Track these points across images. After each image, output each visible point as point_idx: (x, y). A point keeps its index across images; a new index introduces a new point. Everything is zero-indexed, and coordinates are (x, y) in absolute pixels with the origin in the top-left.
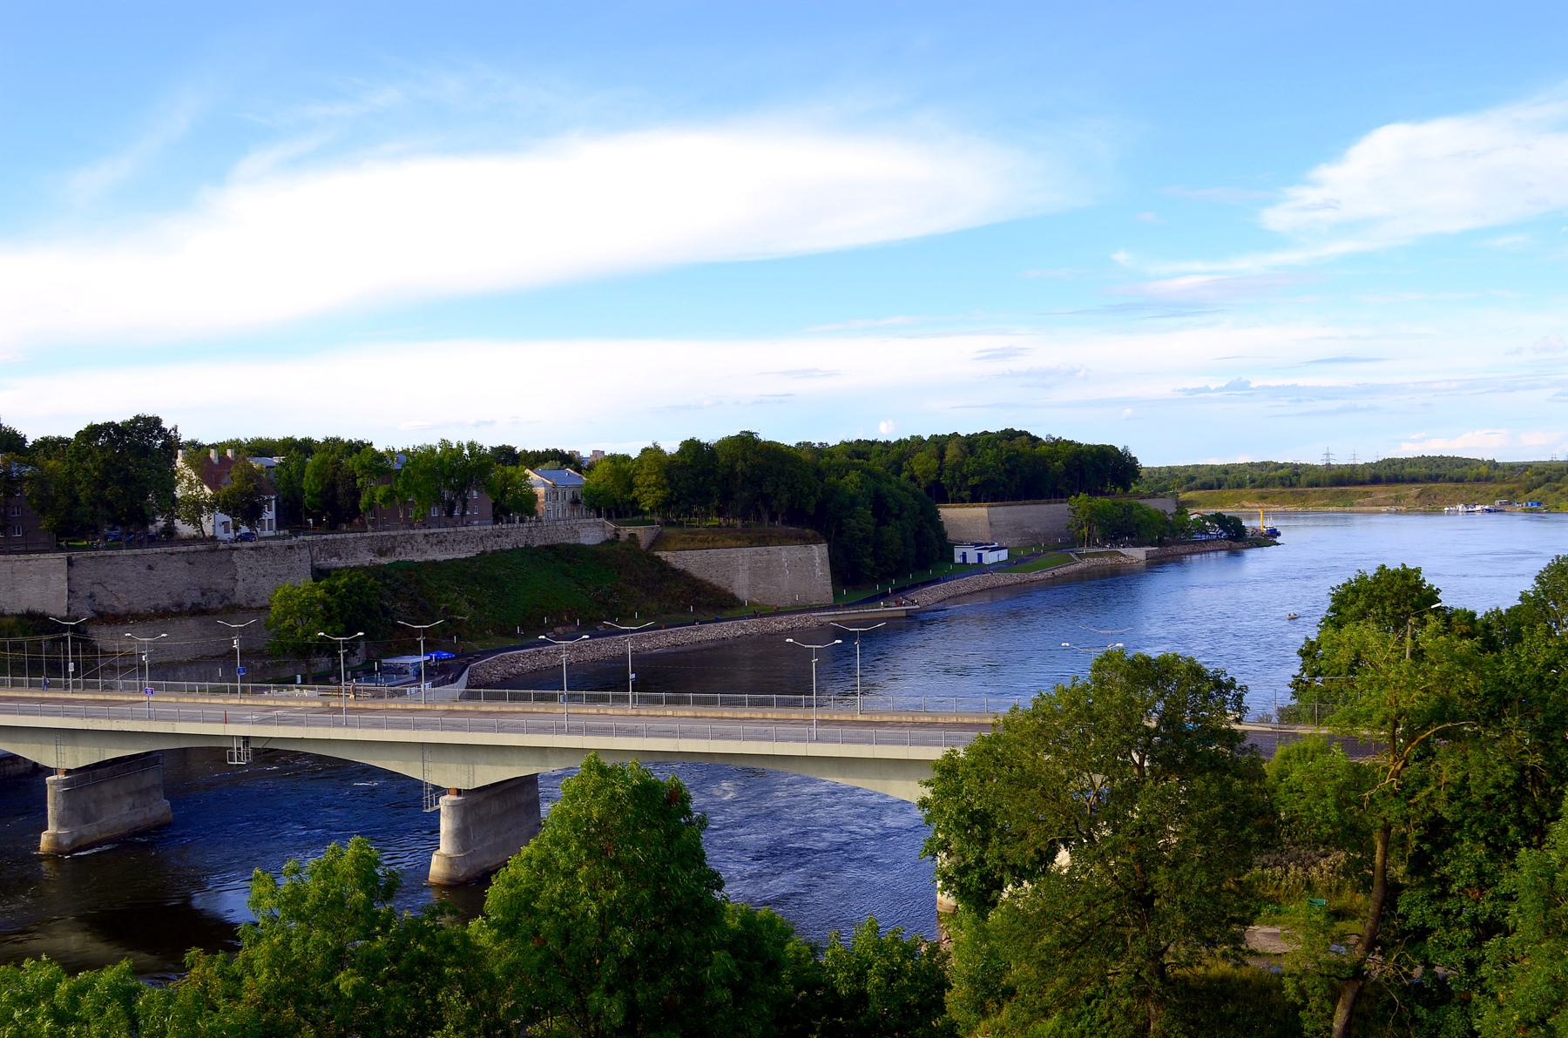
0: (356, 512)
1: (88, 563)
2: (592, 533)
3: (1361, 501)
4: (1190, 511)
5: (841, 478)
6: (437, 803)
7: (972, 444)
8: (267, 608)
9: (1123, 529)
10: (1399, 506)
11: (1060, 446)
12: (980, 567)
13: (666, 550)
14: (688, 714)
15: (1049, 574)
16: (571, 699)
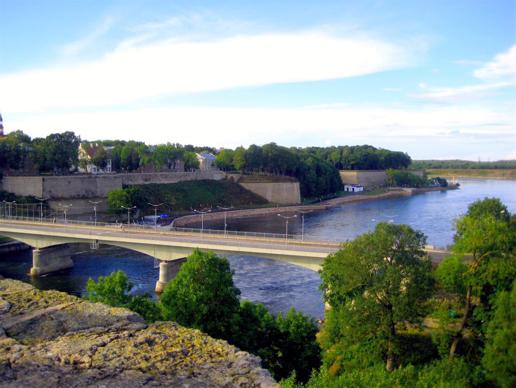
0: (138, 166)
1: (63, 180)
2: (218, 176)
3: (490, 175)
4: (428, 176)
5: (306, 160)
6: (159, 265)
7: (352, 150)
8: (106, 198)
9: (403, 182)
10: (504, 177)
11: (383, 151)
12: (353, 193)
13: (244, 183)
14: (244, 239)
15: (377, 196)
16: (204, 232)
